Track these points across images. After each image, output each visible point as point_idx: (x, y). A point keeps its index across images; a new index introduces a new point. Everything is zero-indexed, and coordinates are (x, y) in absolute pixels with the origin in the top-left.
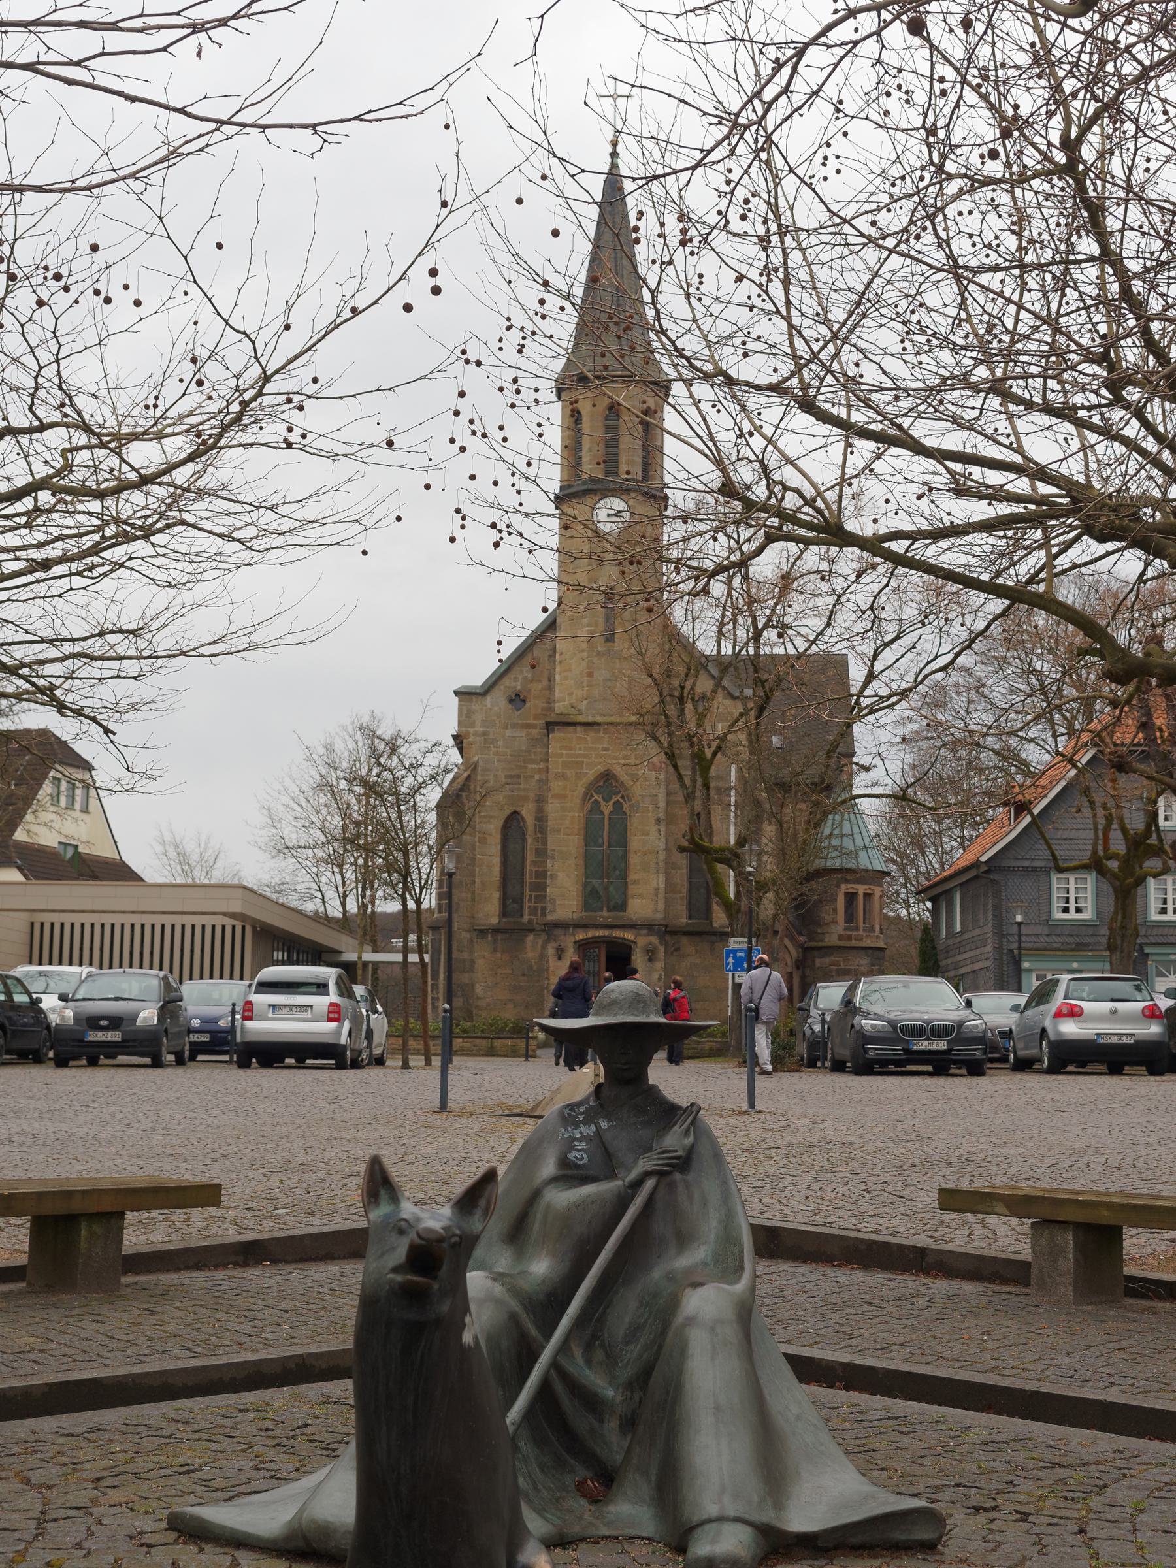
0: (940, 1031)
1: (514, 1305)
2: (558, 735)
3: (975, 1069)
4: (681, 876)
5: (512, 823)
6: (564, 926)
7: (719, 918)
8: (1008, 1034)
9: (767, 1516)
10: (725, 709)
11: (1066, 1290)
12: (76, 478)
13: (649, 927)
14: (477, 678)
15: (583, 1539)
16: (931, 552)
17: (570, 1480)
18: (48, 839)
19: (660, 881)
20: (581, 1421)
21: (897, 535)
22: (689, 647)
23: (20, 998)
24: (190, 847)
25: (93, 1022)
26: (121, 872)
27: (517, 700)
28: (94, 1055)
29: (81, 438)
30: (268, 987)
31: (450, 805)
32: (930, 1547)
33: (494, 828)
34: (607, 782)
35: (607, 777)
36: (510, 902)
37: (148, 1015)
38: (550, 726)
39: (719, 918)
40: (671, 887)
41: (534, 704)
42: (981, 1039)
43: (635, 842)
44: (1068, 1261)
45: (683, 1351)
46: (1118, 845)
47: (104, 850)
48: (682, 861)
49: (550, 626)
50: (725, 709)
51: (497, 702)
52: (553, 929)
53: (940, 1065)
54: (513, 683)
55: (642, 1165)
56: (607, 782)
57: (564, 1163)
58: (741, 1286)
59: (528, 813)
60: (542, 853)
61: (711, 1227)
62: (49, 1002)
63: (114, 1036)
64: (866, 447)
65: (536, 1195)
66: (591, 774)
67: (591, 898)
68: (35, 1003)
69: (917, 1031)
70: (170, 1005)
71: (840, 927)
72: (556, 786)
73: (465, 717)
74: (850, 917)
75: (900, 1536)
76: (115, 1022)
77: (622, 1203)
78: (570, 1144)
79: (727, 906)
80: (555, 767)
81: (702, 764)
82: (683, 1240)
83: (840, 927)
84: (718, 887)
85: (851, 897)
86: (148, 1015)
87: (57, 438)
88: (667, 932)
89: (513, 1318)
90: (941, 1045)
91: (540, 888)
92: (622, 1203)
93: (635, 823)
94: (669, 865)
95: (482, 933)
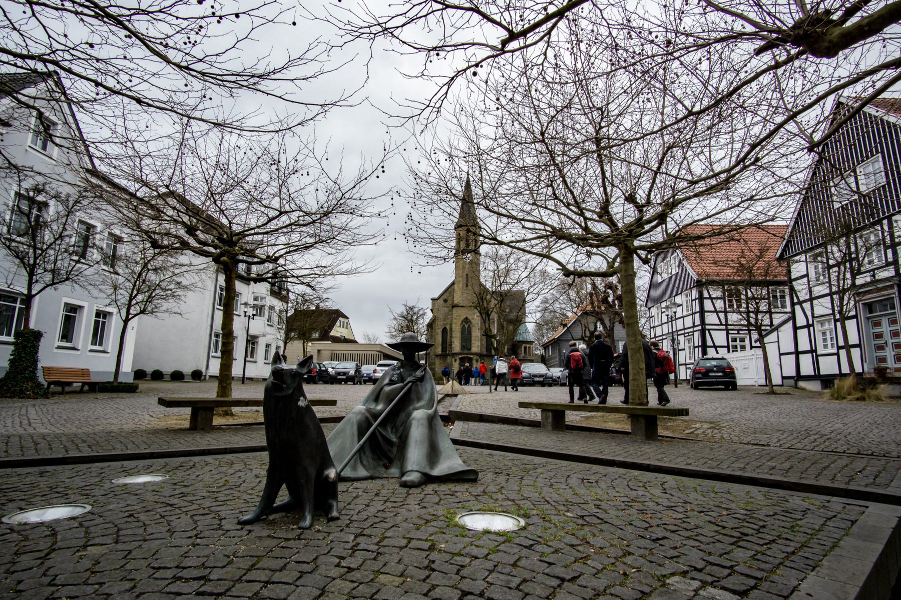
0: (541, 376)
1: (368, 415)
2: (455, 310)
3: (550, 385)
4: (484, 342)
5: (444, 331)
6: (456, 354)
7: (493, 353)
8: (559, 378)
9: (428, 470)
10: (493, 302)
11: (550, 428)
12: (302, 222)
13: (476, 354)
14: (436, 296)
15: (378, 478)
16: (518, 245)
17: (381, 463)
18: (338, 335)
19: (479, 343)
20: (386, 447)
21: (512, 242)
22: (484, 287)
23: (323, 369)
24: (371, 336)
25: (339, 374)
26: (354, 342)
27: (445, 301)
28: (339, 382)
29: (301, 214)
30: (380, 365)
31: (430, 326)
32: (475, 481)
33: (440, 331)
34: (466, 320)
35: (467, 318)
36: (444, 348)
37: (352, 372)
38: (453, 307)
39: (493, 353)
40: (482, 345)
41: (449, 302)
42: (551, 378)
43: (473, 334)
44: (550, 420)
45: (410, 427)
46: (588, 334)
47: (351, 338)
48: (484, 338)
49: (453, 284)
50: (493, 302)
51: (441, 301)
52: (454, 355)
53: (542, 384)
54: (444, 297)
55: (409, 379)
56: (466, 320)
57: (391, 380)
58: (430, 412)
59: (448, 327)
60: (451, 337)
61: (427, 396)
62: (330, 370)
63: (344, 377)
64: (505, 220)
65: (382, 388)
66: (462, 318)
67: (463, 347)
68: (327, 369)
69: (535, 376)
70: (358, 370)
71: (523, 354)
72: (454, 321)
73: (433, 305)
74: (525, 352)
75: (466, 477)
76: (344, 374)
77: (402, 388)
78: (393, 376)
79: (494, 349)
80: (454, 316)
81: (489, 315)
82: (419, 399)
83: (523, 354)
84: (492, 344)
85: (525, 348)
86: (352, 372)
87: (297, 214)
88: (480, 355)
89: (367, 418)
90: (541, 379)
91: (451, 345)
92: (402, 388)
93: (473, 329)
94: (481, 340)
95: (437, 356)
